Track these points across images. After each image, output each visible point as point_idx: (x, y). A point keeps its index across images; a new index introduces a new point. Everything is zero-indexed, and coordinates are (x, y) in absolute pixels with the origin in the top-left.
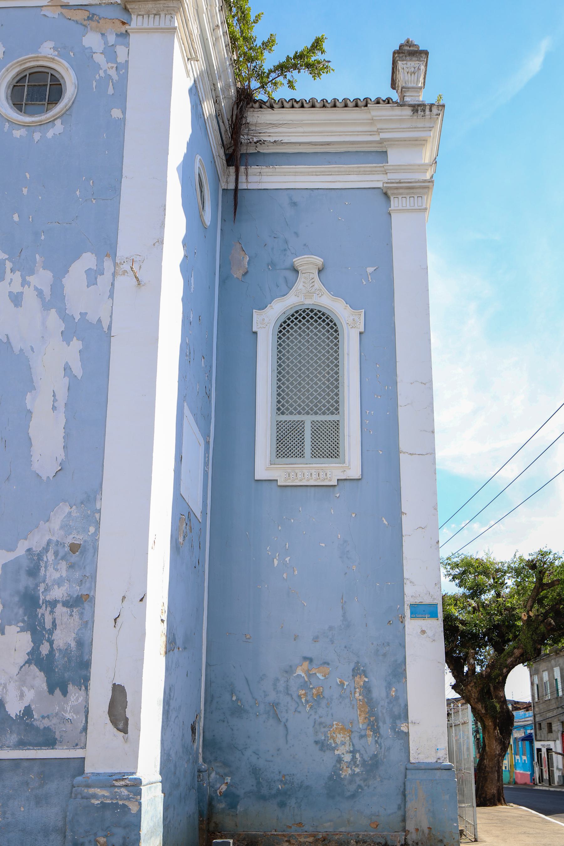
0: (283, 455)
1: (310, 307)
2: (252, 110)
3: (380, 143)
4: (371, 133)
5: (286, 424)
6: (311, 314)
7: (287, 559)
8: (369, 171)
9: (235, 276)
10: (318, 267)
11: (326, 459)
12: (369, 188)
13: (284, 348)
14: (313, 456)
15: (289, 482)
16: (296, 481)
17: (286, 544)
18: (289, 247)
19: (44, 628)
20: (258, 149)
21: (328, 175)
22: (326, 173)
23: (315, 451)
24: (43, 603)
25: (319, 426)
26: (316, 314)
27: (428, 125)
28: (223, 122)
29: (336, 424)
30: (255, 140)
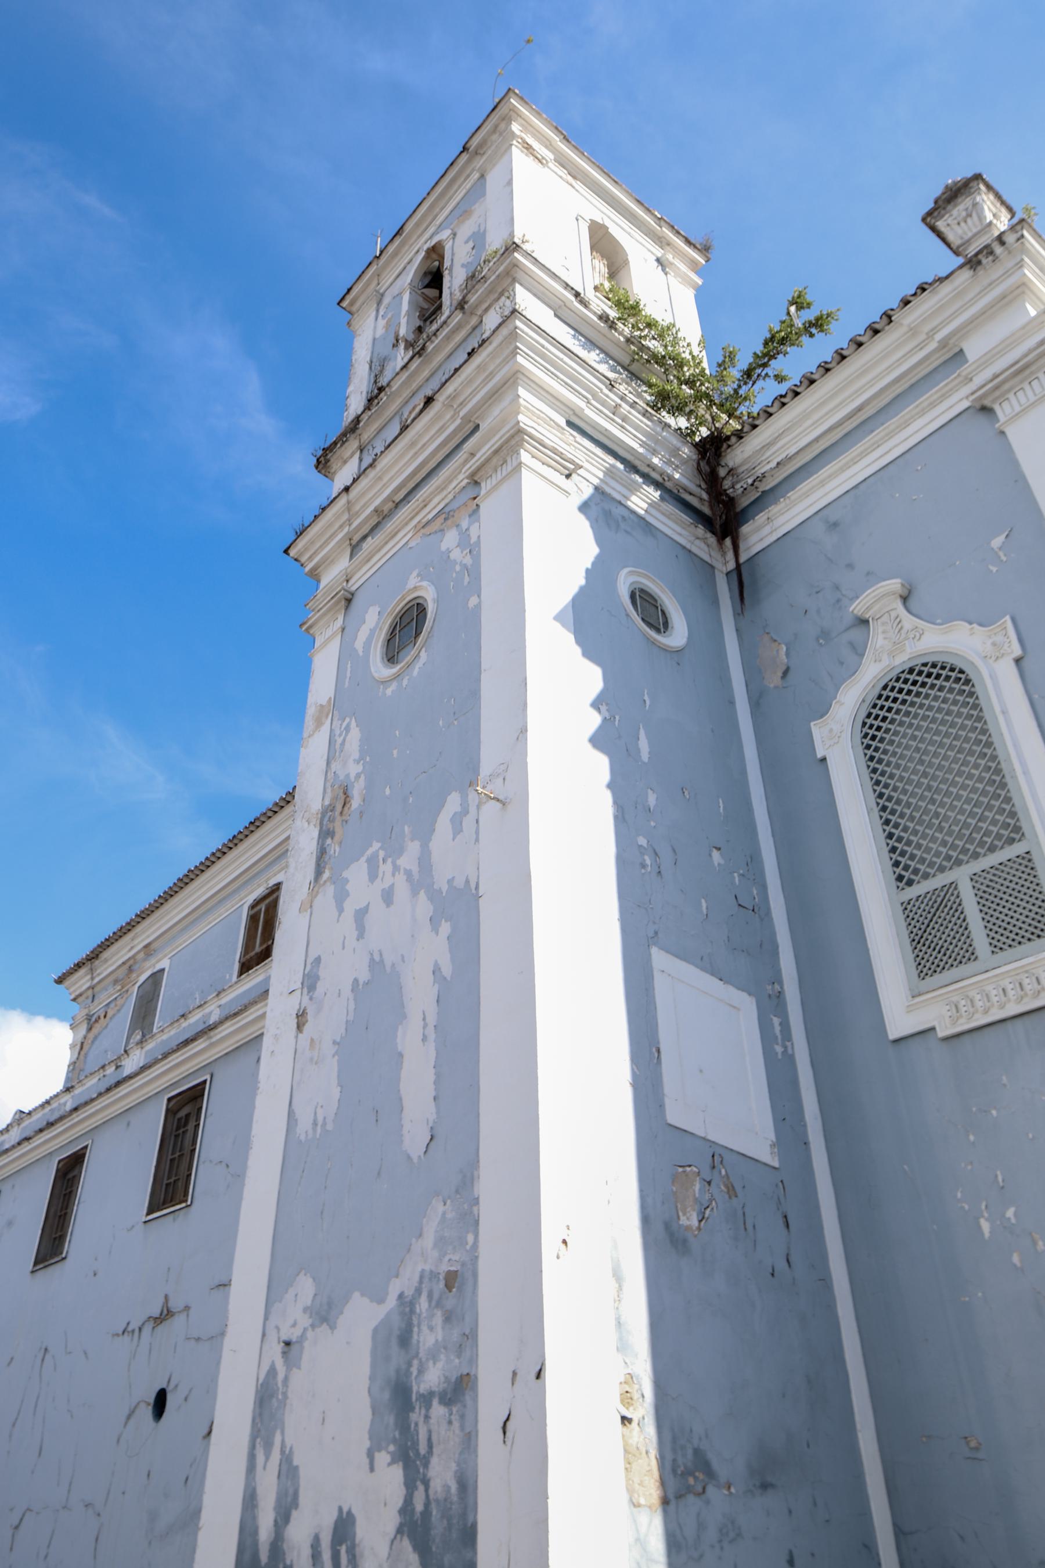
0: (933, 967)
1: (907, 667)
2: (729, 450)
3: (944, 347)
4: (920, 346)
5: (922, 903)
6: (912, 677)
7: (1010, 1213)
8: (938, 399)
9: (772, 686)
10: (897, 595)
11: (1027, 947)
12: (951, 420)
13: (880, 761)
14: (997, 948)
15: (962, 1024)
16: (976, 1016)
17: (996, 1176)
18: (844, 592)
19: (417, 1453)
20: (761, 489)
21: (874, 450)
22: (869, 450)
23: (997, 937)
24: (417, 1400)
25: (991, 881)
26: (920, 673)
27: (1010, 264)
28: (691, 494)
29: (1025, 862)
30: (750, 481)
